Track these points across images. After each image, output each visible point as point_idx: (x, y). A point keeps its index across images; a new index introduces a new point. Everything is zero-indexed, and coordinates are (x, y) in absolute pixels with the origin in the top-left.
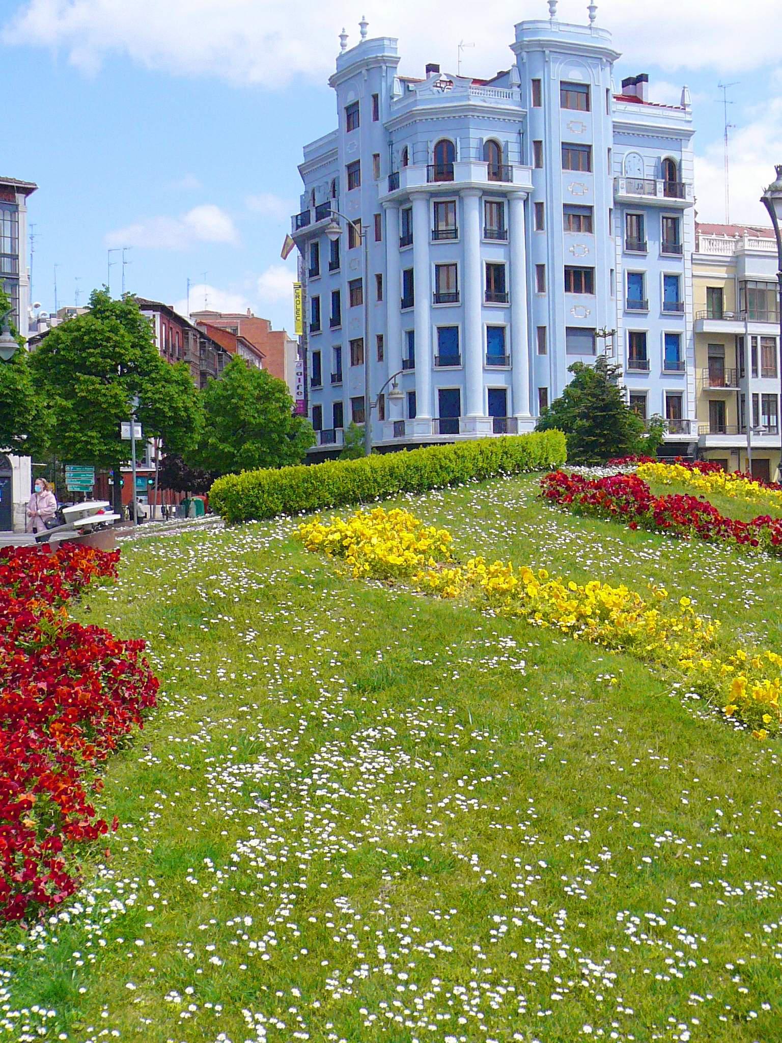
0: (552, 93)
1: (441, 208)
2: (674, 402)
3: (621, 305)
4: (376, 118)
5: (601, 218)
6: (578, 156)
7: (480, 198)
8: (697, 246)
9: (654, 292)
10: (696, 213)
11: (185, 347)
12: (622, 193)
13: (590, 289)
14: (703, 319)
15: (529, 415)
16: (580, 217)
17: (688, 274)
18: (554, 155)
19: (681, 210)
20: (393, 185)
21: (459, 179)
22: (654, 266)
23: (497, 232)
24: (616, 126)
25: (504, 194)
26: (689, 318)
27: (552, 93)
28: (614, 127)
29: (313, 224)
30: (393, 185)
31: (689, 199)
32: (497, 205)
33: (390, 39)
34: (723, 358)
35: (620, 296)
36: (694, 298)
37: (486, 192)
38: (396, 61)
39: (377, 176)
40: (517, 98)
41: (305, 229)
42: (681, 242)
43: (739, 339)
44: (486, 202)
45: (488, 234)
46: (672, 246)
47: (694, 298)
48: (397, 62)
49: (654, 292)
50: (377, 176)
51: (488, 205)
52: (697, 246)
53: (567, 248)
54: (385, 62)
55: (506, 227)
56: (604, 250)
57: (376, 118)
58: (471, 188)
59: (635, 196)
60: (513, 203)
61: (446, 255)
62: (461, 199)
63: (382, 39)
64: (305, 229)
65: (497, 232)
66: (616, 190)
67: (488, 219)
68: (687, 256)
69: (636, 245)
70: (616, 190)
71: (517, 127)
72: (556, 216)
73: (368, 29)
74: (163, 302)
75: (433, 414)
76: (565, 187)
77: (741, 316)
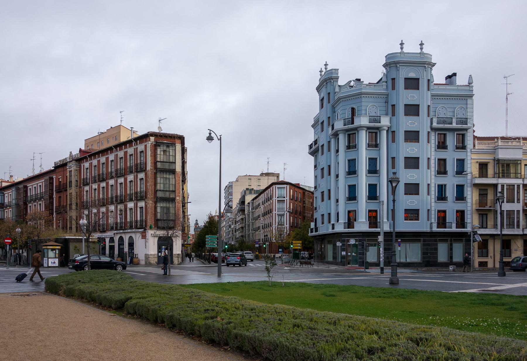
0: (401, 84)
1: (351, 136)
2: (461, 214)
3: (433, 173)
4: (329, 103)
5: (423, 136)
6: (412, 110)
7: (366, 131)
8: (474, 146)
9: (451, 167)
10: (474, 131)
11: (78, 190)
12: (435, 125)
13: (417, 167)
14: (476, 177)
15: (365, 221)
16: (412, 136)
17: (469, 158)
18: (401, 110)
19: (466, 130)
20: (333, 129)
21: (356, 124)
22: (451, 155)
23: (374, 144)
24: (432, 96)
25: (378, 128)
26: (469, 177)
27: (401, 84)
28: (432, 96)
29: (314, 147)
30: (333, 129)
31: (469, 125)
32: (374, 132)
33: (335, 69)
34: (487, 194)
35: (433, 169)
36: (472, 168)
37: (368, 128)
38: (337, 78)
39: (329, 125)
40: (385, 87)
41: (312, 150)
42: (466, 144)
43: (495, 186)
44: (369, 132)
45: (369, 146)
46: (462, 146)
47: (472, 168)
48: (338, 79)
49: (451, 167)
50: (329, 125)
51: (370, 134)
52: (474, 146)
53: (409, 149)
54: (332, 79)
55: (378, 142)
56: (427, 150)
57: (329, 103)
58: (361, 127)
59: (441, 126)
60: (382, 132)
61: (352, 155)
62: (358, 131)
63: (332, 70)
64: (312, 150)
65: (374, 144)
66: (432, 123)
67: (370, 139)
68: (469, 150)
69: (442, 145)
70: (432, 123)
71: (384, 100)
72: (401, 136)
73: (328, 66)
74: (290, 182)
75: (345, 220)
76: (408, 123)
77: (497, 175)
